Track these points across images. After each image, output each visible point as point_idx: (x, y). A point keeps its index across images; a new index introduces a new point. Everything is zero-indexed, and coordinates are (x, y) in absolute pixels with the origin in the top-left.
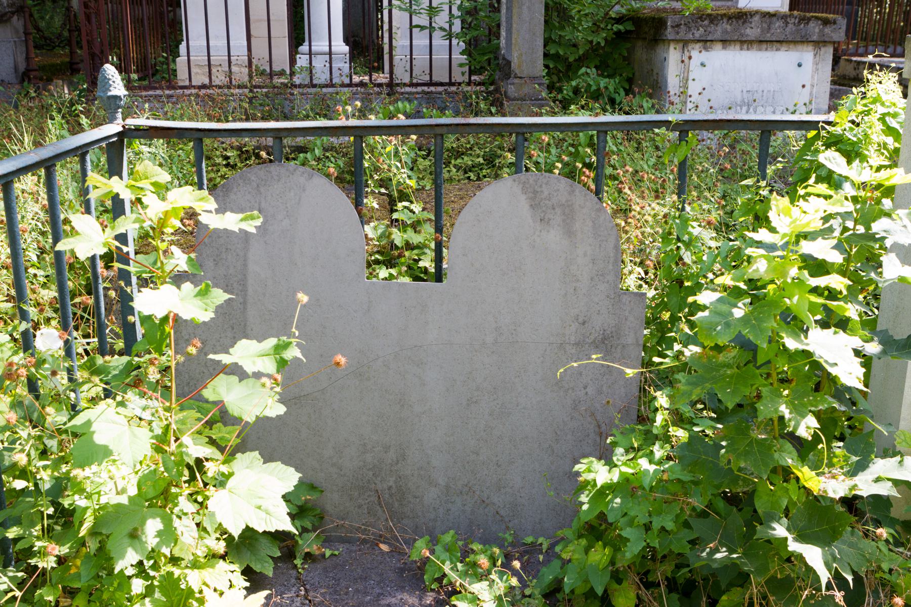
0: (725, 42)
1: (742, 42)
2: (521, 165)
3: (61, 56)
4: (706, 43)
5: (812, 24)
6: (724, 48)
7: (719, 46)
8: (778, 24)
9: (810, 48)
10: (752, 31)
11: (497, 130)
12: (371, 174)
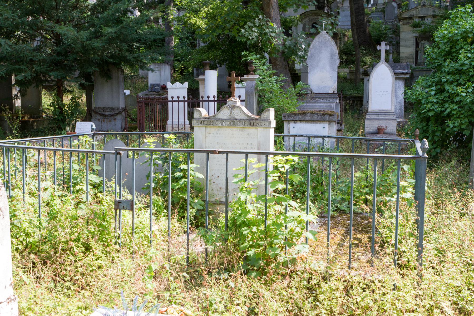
0: (301, 121)
1: (306, 121)
2: (425, 185)
3: (134, 124)
4: (295, 121)
5: (326, 116)
6: (301, 123)
7: (299, 122)
8: (315, 116)
9: (327, 123)
10: (308, 118)
11: (391, 158)
12: (260, 246)
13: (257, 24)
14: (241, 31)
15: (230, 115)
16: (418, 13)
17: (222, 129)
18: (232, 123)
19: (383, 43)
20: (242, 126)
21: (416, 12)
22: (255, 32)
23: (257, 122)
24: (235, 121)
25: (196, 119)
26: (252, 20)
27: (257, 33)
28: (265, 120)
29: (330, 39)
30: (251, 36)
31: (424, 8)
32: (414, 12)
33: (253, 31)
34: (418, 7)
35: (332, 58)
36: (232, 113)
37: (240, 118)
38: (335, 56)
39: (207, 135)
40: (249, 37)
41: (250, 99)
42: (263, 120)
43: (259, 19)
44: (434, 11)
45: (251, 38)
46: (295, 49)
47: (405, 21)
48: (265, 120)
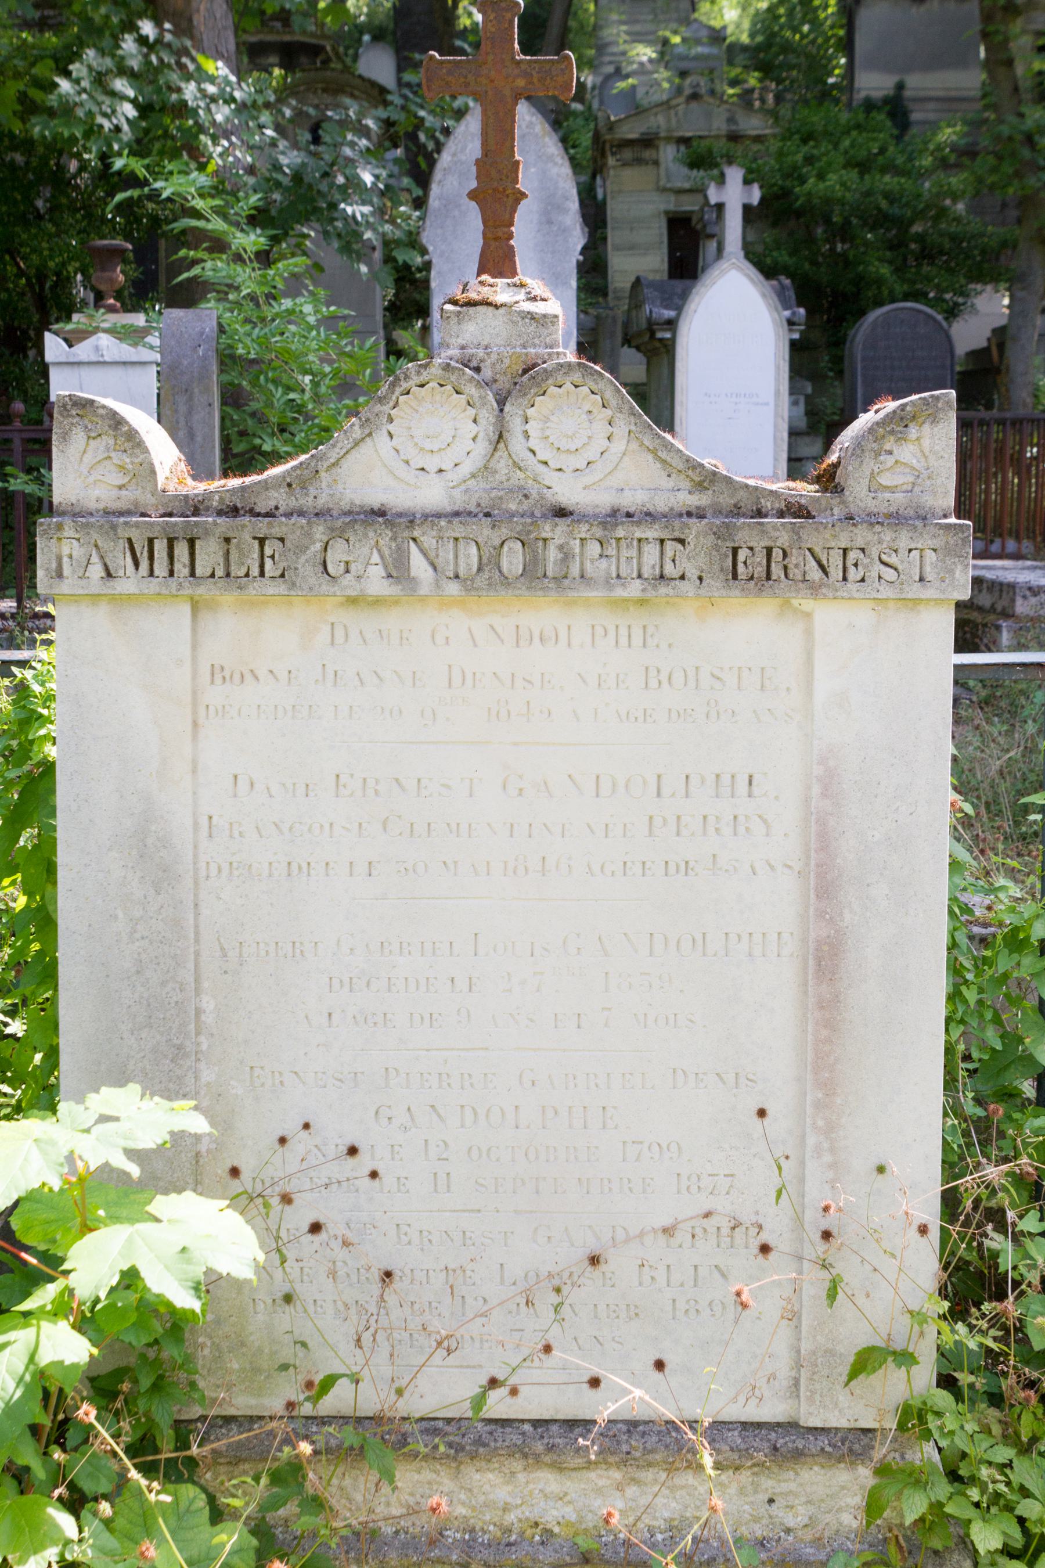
13: (135, 64)
14: (56, 85)
15: (486, 469)
16: (674, 121)
17: (392, 620)
18: (513, 559)
19: (735, 175)
20: (635, 589)
21: (669, 121)
22: (124, 98)
23: (813, 539)
24: (556, 532)
25: (77, 513)
26: (107, 42)
27: (134, 102)
28: (896, 519)
29: (538, 129)
30: (105, 115)
31: (694, 105)
32: (661, 119)
33: (113, 94)
34: (674, 102)
35: (550, 222)
36: (517, 444)
37: (602, 500)
38: (566, 211)
39: (214, 695)
40: (100, 120)
41: (190, 412)
42: (873, 520)
43: (142, 40)
44: (731, 120)
45: (107, 125)
46: (324, 187)
47: (628, 154)
48: (896, 519)
